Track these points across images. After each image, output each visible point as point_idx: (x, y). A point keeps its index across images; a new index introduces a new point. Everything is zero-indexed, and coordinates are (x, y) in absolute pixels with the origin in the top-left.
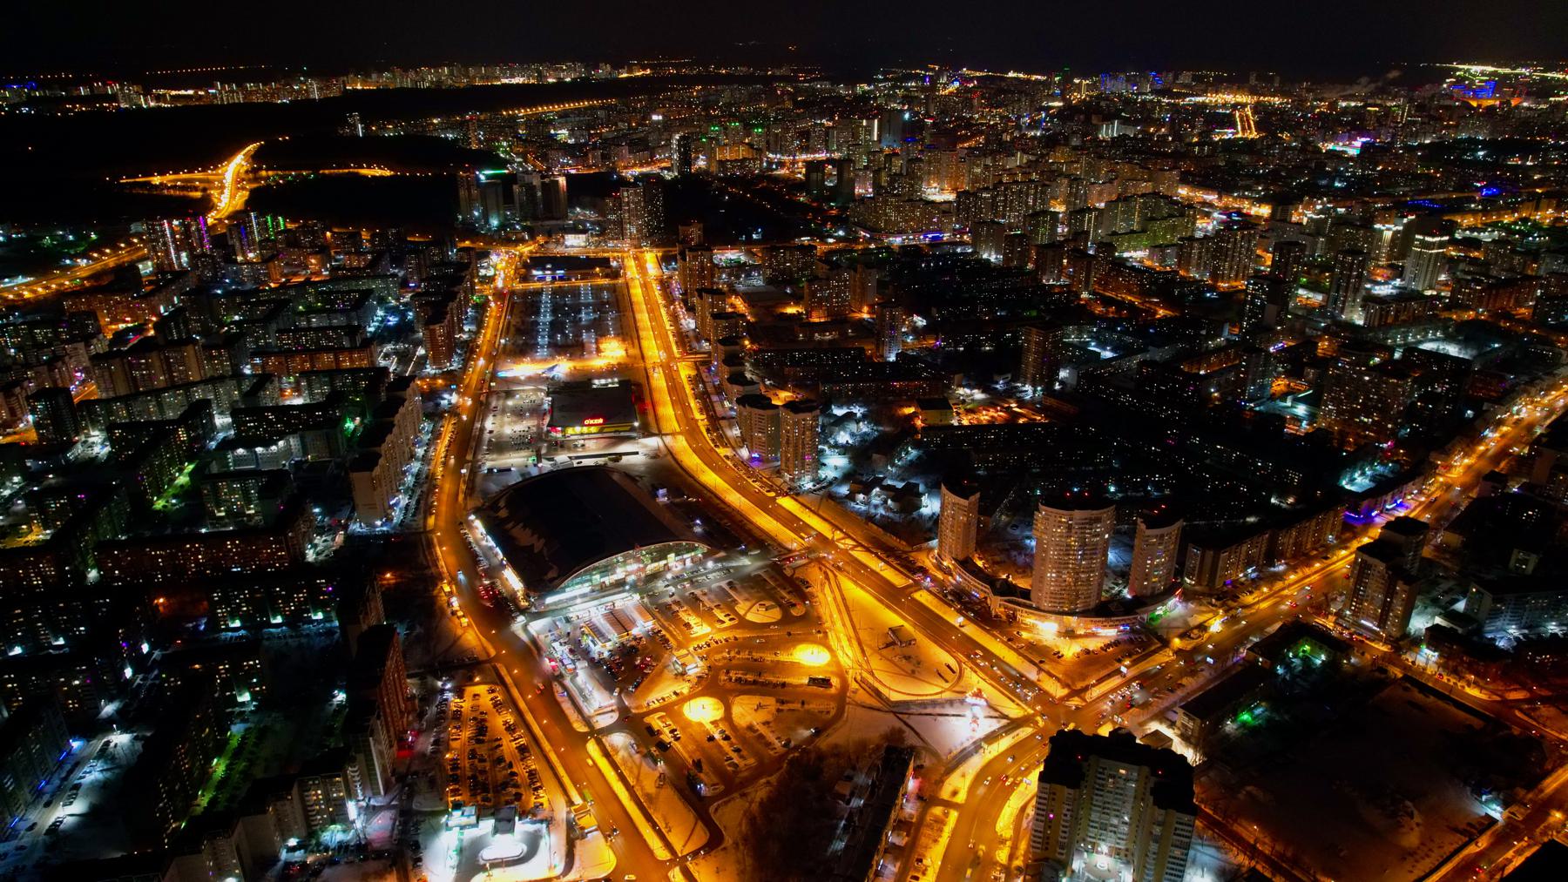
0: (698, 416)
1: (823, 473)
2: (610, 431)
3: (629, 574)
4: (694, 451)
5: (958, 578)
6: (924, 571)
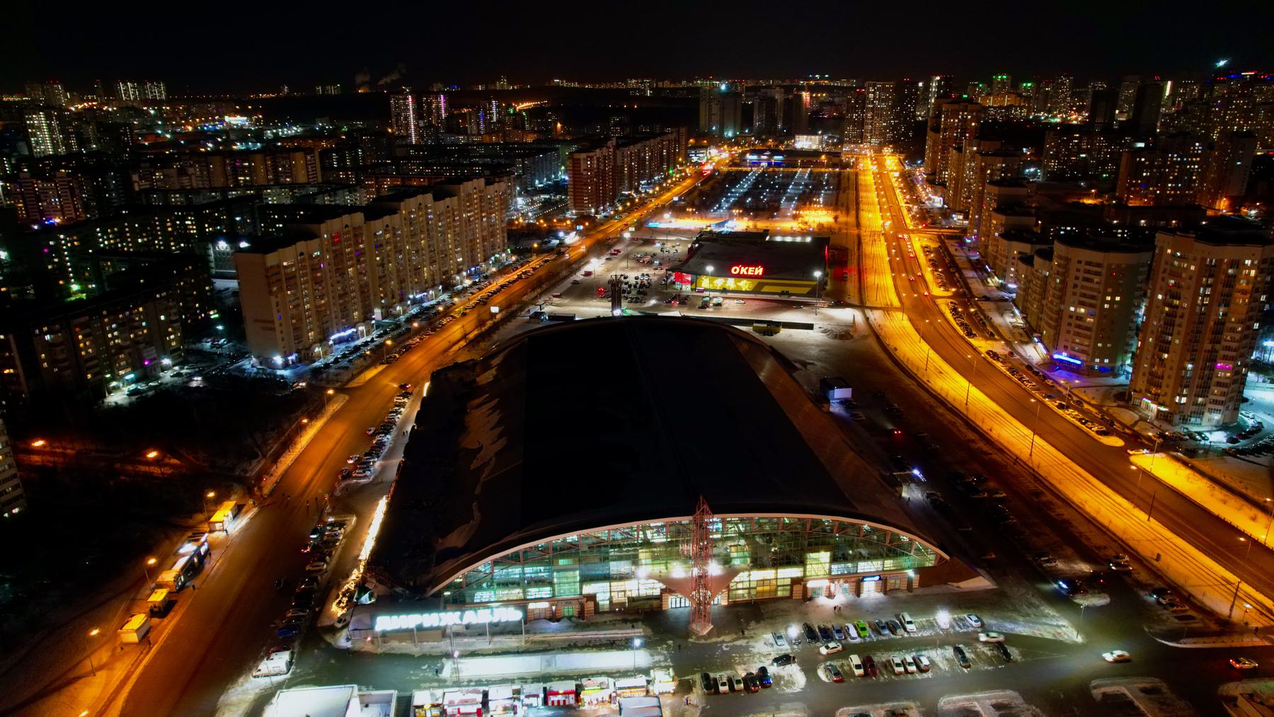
0: (937, 291)
2: (773, 289)
3: (671, 587)
4: (924, 337)
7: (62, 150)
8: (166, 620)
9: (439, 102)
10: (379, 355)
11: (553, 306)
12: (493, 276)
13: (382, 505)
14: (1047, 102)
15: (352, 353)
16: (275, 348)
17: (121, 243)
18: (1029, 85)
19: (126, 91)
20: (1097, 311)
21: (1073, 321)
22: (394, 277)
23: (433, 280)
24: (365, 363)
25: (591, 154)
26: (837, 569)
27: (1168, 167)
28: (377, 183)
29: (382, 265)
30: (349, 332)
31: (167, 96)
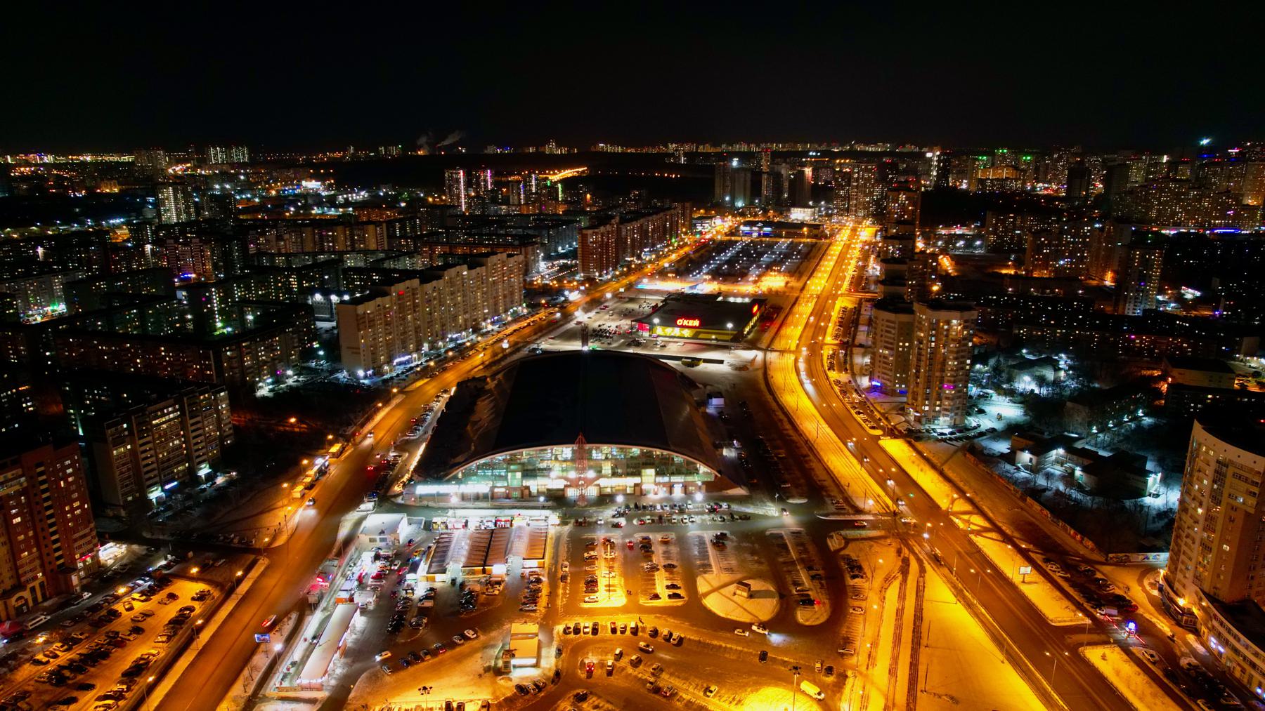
1: (972, 421)
5: (1213, 642)
6: (1127, 609)
7: (184, 217)
8: (312, 491)
9: (487, 176)
10: (425, 372)
11: (546, 345)
12: (510, 323)
13: (423, 446)
14: (1040, 174)
15: (408, 371)
16: (359, 366)
17: (248, 294)
18: (1029, 158)
19: (216, 154)
20: (894, 352)
21: (882, 359)
22: (438, 322)
23: (466, 325)
24: (416, 378)
25: (596, 230)
26: (660, 479)
27: (1064, 245)
28: (430, 249)
29: (430, 314)
30: (407, 358)
31: (250, 158)
